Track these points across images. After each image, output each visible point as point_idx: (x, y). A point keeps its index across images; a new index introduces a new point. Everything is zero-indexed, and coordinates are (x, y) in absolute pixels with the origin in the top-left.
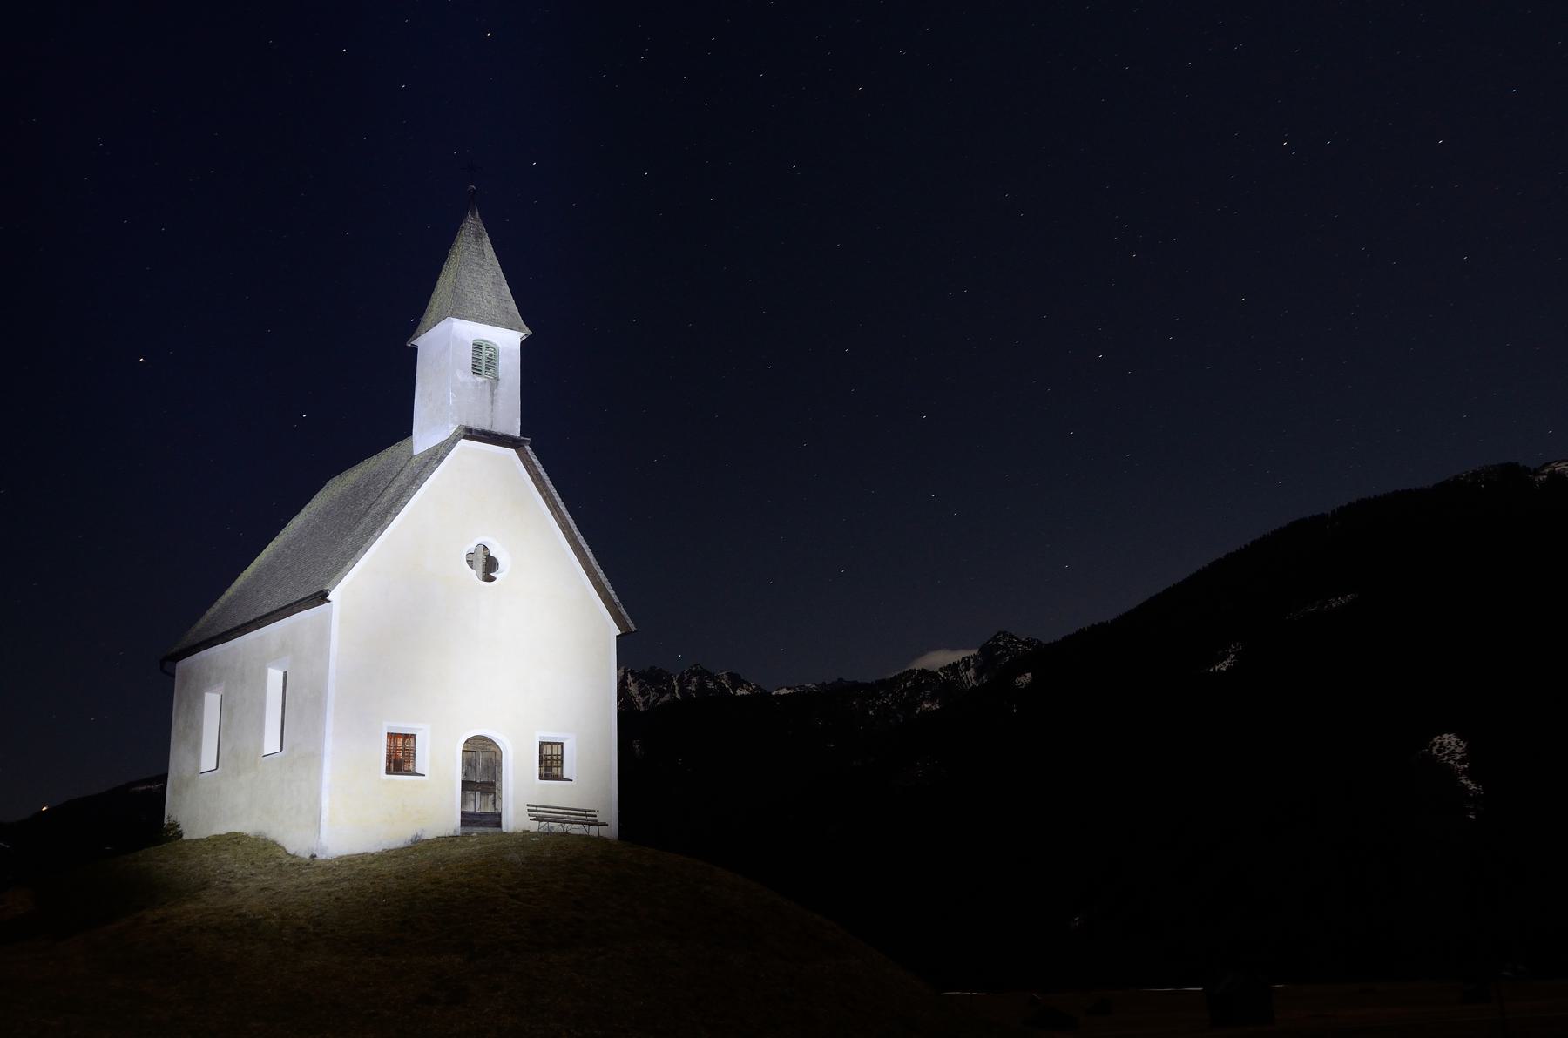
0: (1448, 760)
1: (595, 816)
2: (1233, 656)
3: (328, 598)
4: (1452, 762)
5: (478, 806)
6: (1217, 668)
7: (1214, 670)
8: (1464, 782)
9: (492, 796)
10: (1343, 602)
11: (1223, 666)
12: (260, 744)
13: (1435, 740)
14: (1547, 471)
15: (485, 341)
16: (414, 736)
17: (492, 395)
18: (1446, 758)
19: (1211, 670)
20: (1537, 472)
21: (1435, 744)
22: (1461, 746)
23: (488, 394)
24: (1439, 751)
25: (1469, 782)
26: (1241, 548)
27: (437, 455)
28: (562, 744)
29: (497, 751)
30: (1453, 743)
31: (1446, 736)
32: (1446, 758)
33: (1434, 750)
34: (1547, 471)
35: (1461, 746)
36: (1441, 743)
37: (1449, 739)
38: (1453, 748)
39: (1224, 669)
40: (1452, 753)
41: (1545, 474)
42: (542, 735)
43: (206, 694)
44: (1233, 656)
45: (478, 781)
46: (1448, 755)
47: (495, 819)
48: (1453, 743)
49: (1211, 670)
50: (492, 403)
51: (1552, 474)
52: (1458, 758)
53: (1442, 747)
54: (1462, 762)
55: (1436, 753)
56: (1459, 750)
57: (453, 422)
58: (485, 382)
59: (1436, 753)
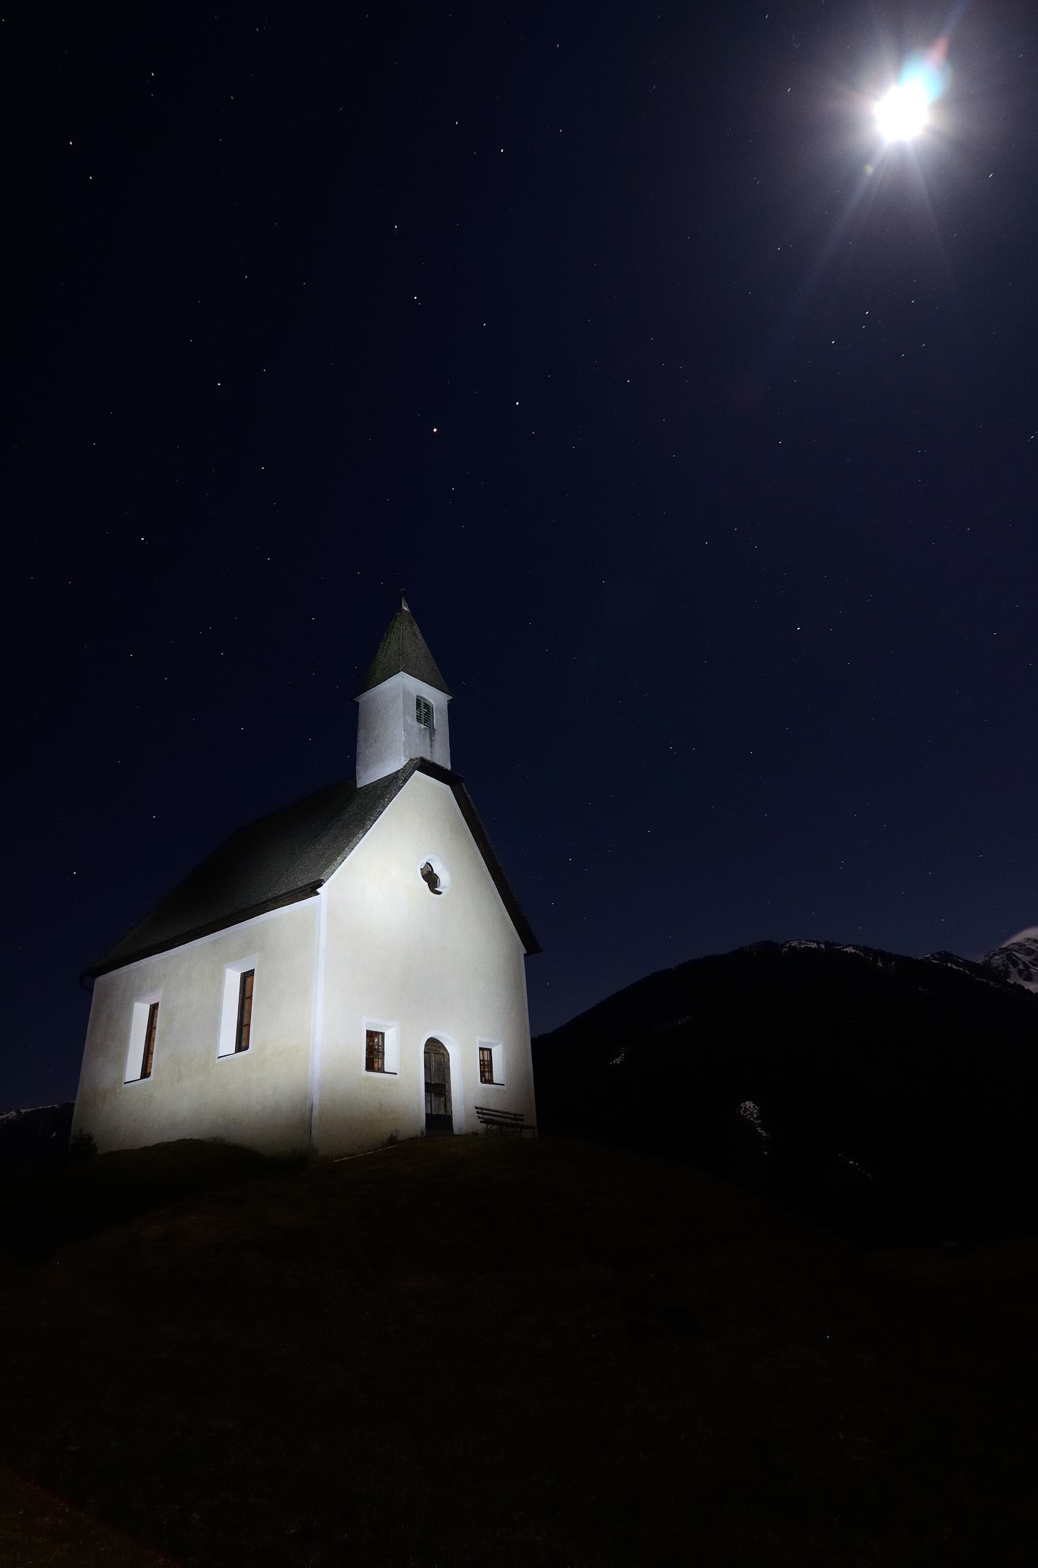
0: (750, 1118)
1: (523, 1120)
2: (623, 1055)
3: (318, 890)
4: (752, 1119)
5: (433, 1110)
6: (614, 1062)
7: (613, 1063)
8: (759, 1131)
9: (443, 1098)
10: (685, 1021)
11: (618, 1061)
12: (122, 1069)
13: (742, 1105)
14: (787, 945)
15: (424, 699)
16: (383, 1034)
17: (431, 740)
18: (749, 1116)
19: (611, 1063)
20: (783, 946)
21: (741, 1108)
22: (756, 1109)
23: (428, 740)
24: (743, 1111)
25: (762, 1131)
26: (628, 987)
27: (391, 785)
28: (490, 1050)
29: (446, 1054)
30: (752, 1107)
31: (747, 1102)
32: (749, 1116)
33: (741, 1111)
34: (787, 945)
35: (756, 1109)
36: (745, 1107)
37: (749, 1104)
38: (752, 1110)
39: (618, 1062)
40: (751, 1113)
41: (786, 948)
42: (482, 1040)
43: (227, 970)
44: (623, 1055)
45: (433, 1083)
46: (749, 1114)
47: (448, 1118)
48: (752, 1107)
49: (611, 1063)
50: (432, 753)
51: (790, 947)
52: (755, 1116)
53: (746, 1110)
54: (757, 1118)
55: (742, 1113)
56: (755, 1111)
57: (405, 756)
58: (426, 728)
59: (742, 1113)
